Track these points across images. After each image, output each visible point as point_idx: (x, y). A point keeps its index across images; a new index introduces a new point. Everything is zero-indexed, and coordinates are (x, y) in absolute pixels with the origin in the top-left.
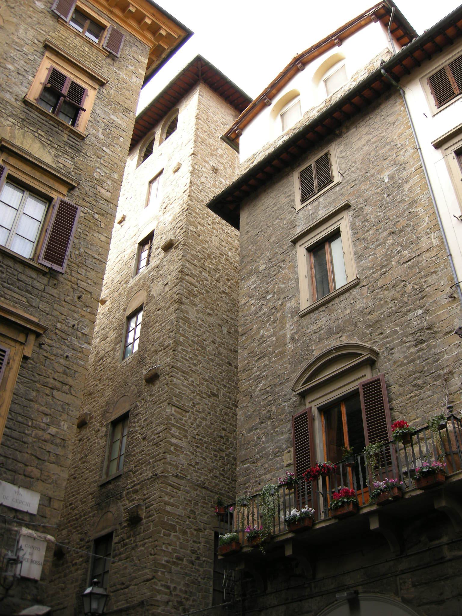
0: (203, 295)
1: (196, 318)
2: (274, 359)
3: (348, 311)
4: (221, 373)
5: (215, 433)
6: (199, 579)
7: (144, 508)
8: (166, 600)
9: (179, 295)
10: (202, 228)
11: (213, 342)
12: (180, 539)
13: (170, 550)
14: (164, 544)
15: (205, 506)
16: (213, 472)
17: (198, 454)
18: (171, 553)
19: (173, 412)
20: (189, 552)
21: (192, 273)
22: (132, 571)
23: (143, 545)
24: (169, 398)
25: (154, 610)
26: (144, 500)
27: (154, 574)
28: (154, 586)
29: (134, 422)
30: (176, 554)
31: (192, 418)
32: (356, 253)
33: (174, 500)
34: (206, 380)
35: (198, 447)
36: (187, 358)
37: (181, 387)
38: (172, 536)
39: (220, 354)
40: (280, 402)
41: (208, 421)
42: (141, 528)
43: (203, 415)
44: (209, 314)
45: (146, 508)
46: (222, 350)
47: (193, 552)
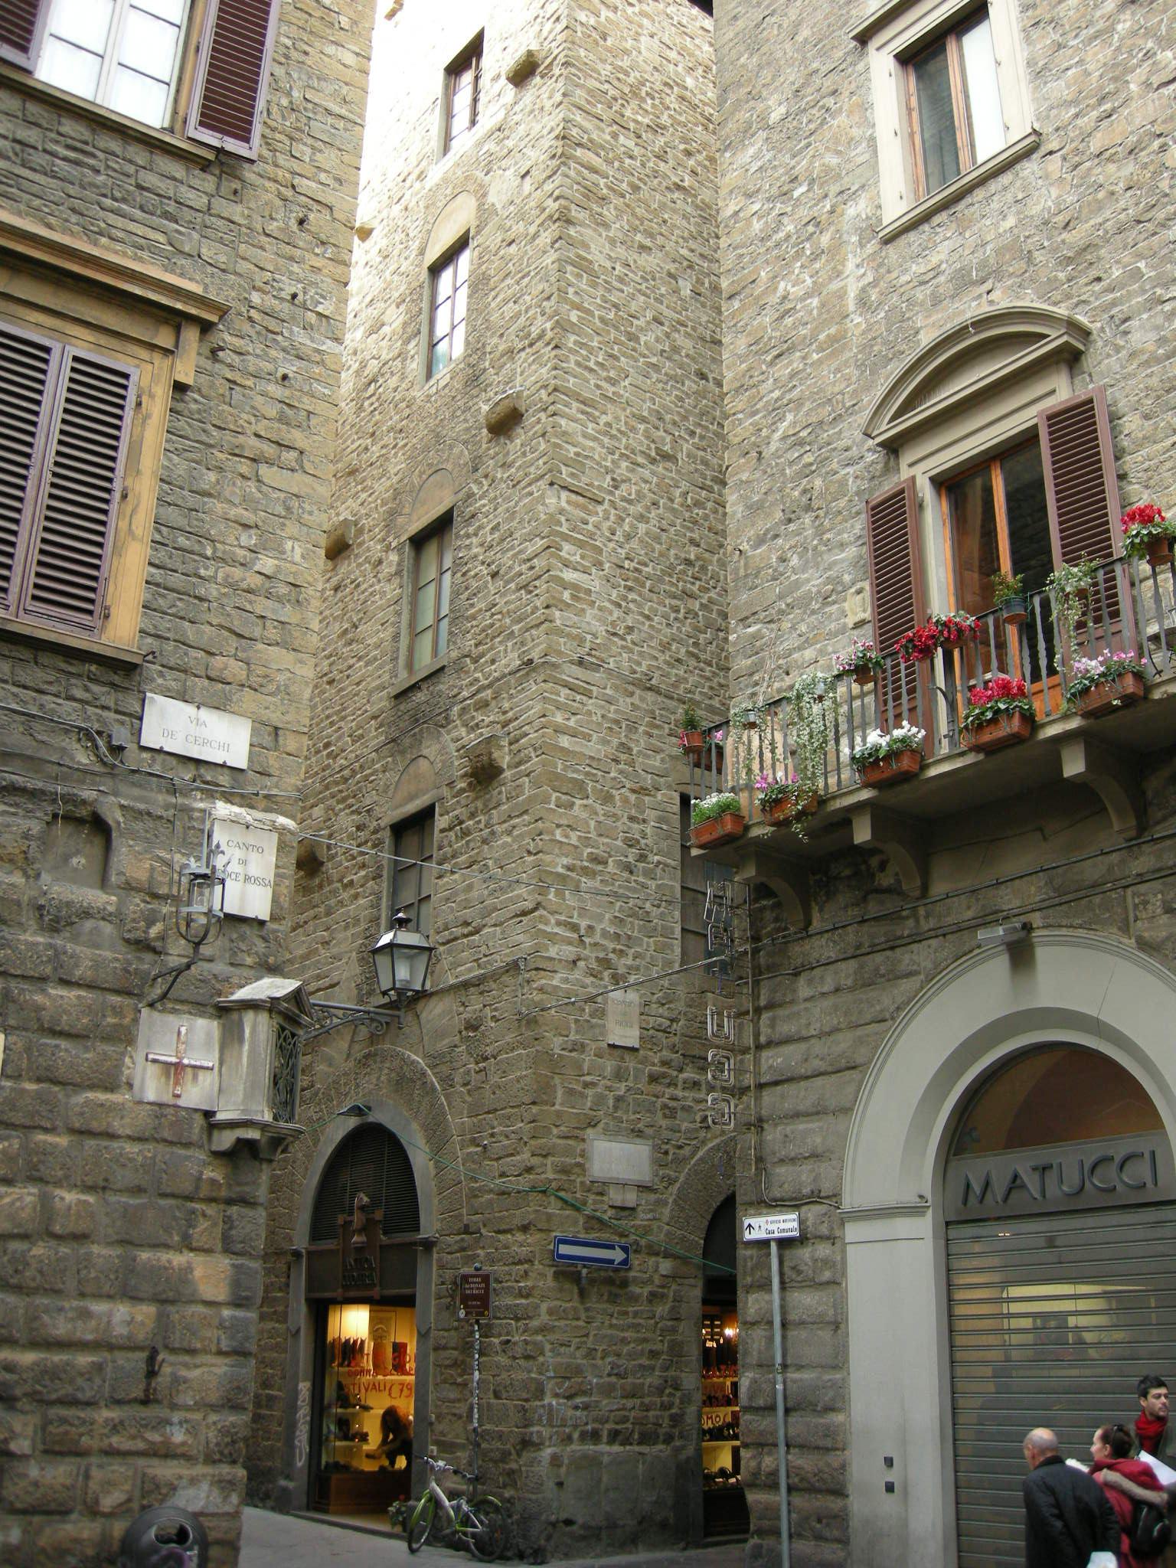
0: (623, 196)
1: (610, 258)
2: (815, 356)
3: (1011, 221)
4: (681, 400)
5: (672, 552)
6: (648, 905)
7: (505, 743)
8: (572, 957)
9: (562, 201)
10: (611, 15)
11: (656, 320)
12: (596, 814)
13: (574, 841)
14: (558, 826)
15: (655, 732)
16: (669, 650)
17: (631, 605)
18: (576, 847)
19: (564, 504)
20: (619, 843)
21: (591, 141)
22: (486, 892)
23: (509, 833)
24: (550, 471)
25: (544, 981)
26: (505, 724)
27: (540, 898)
28: (541, 926)
29: (468, 536)
30: (589, 850)
31: (612, 518)
32: (1030, 63)
33: (576, 722)
34: (643, 420)
35: (630, 589)
36: (591, 364)
37: (581, 439)
38: (576, 808)
39: (676, 349)
40: (835, 466)
41: (653, 522)
42: (500, 793)
43: (639, 508)
44: (643, 248)
45: (511, 744)
46: (680, 339)
47: (631, 843)
